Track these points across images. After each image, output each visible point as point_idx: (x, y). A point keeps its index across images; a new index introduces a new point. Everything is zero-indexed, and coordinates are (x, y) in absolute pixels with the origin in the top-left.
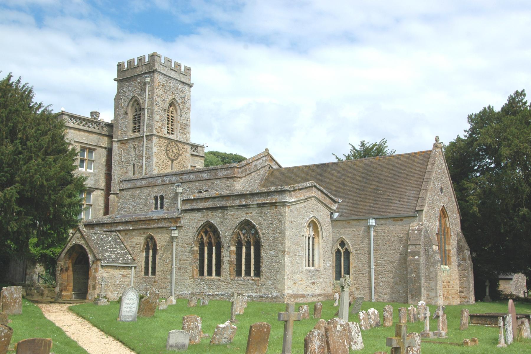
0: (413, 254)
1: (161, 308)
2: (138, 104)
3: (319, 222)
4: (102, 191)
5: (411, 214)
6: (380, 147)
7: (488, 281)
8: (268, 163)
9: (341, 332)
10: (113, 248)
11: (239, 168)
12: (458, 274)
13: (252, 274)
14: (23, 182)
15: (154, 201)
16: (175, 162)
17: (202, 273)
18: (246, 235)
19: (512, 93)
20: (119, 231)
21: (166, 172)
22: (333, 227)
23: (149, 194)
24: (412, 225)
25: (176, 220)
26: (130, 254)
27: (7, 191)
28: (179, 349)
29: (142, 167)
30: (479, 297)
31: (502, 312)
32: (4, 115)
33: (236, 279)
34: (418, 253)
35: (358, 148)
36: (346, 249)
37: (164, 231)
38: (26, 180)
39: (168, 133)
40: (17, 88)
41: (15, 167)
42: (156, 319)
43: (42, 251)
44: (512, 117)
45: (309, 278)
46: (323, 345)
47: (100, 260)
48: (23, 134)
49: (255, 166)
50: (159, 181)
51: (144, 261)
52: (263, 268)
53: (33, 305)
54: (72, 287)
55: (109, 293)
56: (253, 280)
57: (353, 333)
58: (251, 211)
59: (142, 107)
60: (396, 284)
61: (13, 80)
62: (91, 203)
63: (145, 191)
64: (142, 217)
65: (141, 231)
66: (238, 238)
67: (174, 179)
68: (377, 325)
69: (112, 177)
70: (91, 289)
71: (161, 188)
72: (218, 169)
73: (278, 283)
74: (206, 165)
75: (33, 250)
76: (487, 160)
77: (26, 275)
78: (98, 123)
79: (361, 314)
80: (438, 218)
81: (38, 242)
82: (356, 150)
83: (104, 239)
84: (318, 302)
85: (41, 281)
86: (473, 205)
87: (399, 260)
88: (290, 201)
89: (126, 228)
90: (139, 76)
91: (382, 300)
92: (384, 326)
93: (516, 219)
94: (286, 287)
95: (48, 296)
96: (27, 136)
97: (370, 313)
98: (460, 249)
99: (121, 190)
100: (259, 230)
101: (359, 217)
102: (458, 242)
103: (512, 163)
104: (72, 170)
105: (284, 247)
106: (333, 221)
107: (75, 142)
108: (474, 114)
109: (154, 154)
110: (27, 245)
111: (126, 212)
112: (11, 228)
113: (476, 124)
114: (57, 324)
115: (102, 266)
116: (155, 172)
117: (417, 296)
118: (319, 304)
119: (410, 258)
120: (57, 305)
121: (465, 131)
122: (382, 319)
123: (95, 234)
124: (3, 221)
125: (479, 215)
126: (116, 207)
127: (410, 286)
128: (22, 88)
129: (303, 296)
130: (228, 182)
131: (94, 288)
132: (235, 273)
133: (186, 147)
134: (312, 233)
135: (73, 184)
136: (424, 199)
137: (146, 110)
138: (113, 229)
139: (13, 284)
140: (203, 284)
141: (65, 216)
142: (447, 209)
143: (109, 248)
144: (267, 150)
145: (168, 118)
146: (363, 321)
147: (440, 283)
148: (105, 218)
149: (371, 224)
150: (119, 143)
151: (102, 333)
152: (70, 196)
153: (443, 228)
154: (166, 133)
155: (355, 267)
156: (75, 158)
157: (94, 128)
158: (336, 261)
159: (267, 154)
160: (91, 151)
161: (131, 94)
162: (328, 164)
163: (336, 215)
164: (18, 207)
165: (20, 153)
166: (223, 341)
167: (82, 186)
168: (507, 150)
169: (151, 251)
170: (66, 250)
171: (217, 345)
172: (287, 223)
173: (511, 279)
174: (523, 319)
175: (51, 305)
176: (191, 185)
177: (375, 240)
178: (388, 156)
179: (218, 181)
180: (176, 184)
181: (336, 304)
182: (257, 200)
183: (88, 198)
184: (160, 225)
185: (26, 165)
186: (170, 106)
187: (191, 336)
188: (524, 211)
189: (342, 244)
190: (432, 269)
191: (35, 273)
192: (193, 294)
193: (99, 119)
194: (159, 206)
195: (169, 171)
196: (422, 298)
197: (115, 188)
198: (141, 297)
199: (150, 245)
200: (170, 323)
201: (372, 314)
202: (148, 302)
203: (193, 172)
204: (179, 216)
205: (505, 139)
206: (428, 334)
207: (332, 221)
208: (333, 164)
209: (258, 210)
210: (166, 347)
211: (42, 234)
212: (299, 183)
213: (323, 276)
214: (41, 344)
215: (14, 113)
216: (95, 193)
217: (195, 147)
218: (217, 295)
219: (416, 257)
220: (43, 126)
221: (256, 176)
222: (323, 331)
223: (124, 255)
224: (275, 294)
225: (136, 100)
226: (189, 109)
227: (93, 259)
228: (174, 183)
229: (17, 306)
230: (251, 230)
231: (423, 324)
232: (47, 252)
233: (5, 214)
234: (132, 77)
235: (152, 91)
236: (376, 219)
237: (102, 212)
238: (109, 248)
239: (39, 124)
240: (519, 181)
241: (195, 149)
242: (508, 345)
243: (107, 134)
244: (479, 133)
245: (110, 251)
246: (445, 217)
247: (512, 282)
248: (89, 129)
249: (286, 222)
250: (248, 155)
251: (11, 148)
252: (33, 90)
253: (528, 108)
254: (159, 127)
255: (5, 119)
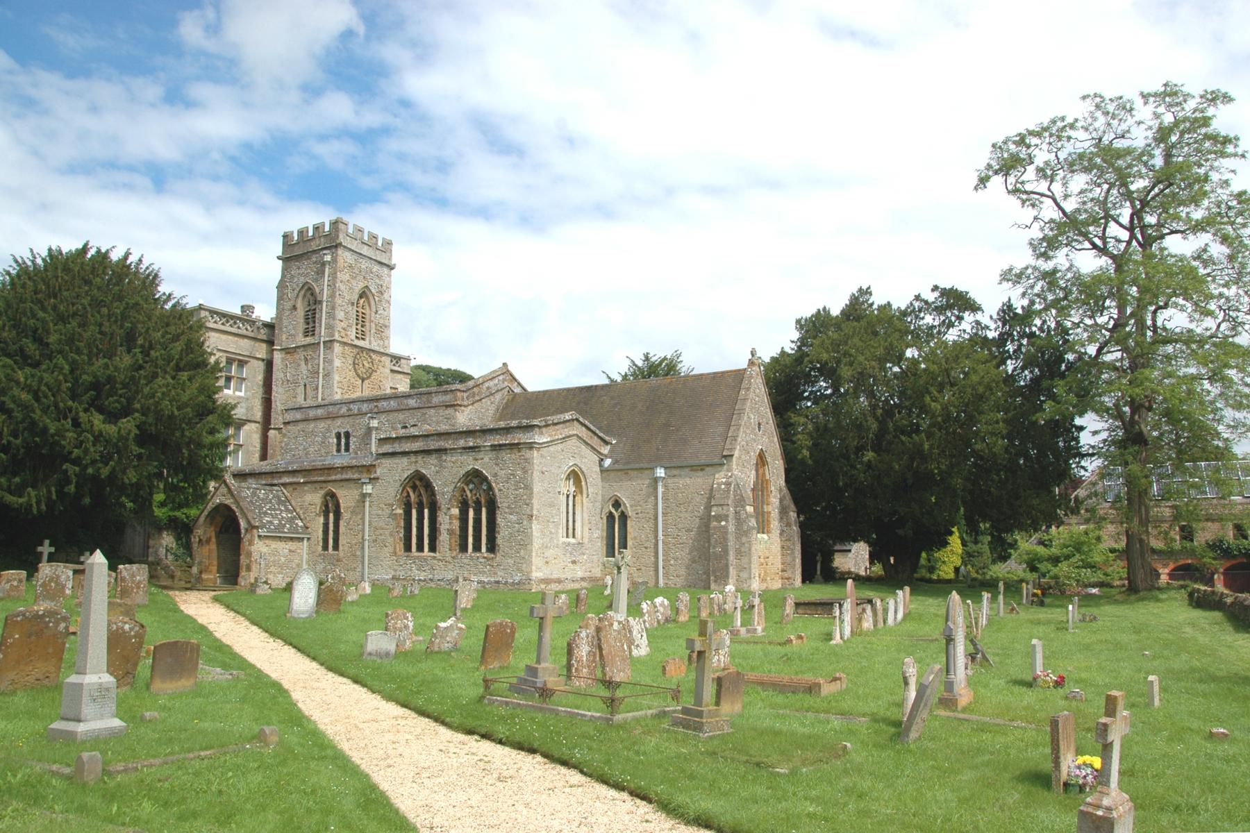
0: (719, 518)
1: (349, 599)
2: (312, 294)
3: (583, 472)
4: (257, 425)
5: (716, 460)
6: (671, 363)
7: (819, 554)
8: (506, 383)
9: (619, 632)
10: (275, 510)
11: (463, 391)
12: (780, 545)
13: (484, 549)
14: (145, 411)
15: (335, 440)
16: (366, 381)
17: (408, 548)
18: (474, 492)
19: (855, 291)
20: (284, 485)
21: (354, 396)
22: (603, 479)
23: (328, 430)
24: (717, 476)
25: (370, 468)
26: (301, 519)
27: (123, 423)
28: (381, 658)
29: (317, 389)
30: (808, 576)
31: (837, 597)
32: (119, 312)
33: (459, 556)
34: (726, 518)
35: (640, 363)
36: (623, 513)
37: (352, 485)
38: (148, 409)
39: (357, 337)
40: (137, 272)
41: (134, 388)
42: (342, 615)
43: (171, 514)
44: (855, 323)
45: (568, 555)
46: (594, 650)
47: (257, 527)
48: (145, 339)
49: (488, 388)
50: (344, 410)
51: (321, 529)
52: (499, 541)
53: (161, 592)
54: (216, 568)
55: (271, 576)
56: (484, 558)
57: (634, 633)
58: (481, 456)
59: (319, 299)
60: (694, 562)
61: (133, 259)
62: (241, 443)
63: (322, 425)
64: (319, 464)
65: (317, 486)
66: (462, 496)
67: (365, 407)
68: (667, 620)
69: (273, 404)
70: (244, 570)
71: (346, 420)
72: (431, 393)
73: (523, 562)
74: (412, 387)
75: (159, 512)
76: (822, 383)
77: (148, 547)
78: (253, 322)
79: (644, 606)
80: (754, 467)
81: (165, 500)
82: (636, 366)
83: (261, 496)
84: (582, 589)
85: (170, 557)
86: (803, 448)
87: (698, 528)
88: (541, 441)
89: (295, 480)
90: (314, 252)
91: (673, 586)
92: (677, 622)
93: (859, 466)
94: (534, 568)
95: (180, 580)
96: (150, 342)
97: (658, 605)
98: (783, 511)
99: (286, 423)
100: (494, 485)
101: (642, 465)
102: (781, 501)
103: (856, 389)
104: (215, 393)
105: (532, 510)
106: (603, 471)
107: (219, 350)
108: (804, 317)
109: (335, 368)
110: (151, 505)
111: (294, 455)
112: (128, 478)
113: (807, 331)
114: (200, 621)
115: (259, 536)
116: (338, 397)
117: (723, 578)
118: (583, 592)
119: (714, 524)
120: (195, 593)
121: (793, 342)
122: (674, 612)
123: (248, 488)
124: (117, 469)
125: (810, 462)
126: (278, 449)
127: (714, 564)
128: (145, 271)
129: (559, 581)
130: (447, 412)
131: (249, 569)
132: (458, 548)
133: (384, 358)
134: (573, 489)
135: (216, 415)
136: (735, 438)
137: (324, 304)
138: (276, 482)
139: (131, 562)
140: (411, 564)
141: (205, 461)
142: (766, 454)
143: (269, 509)
144: (505, 364)
145: (357, 316)
146: (647, 615)
147: (755, 558)
148: (262, 465)
149: (658, 475)
150: (284, 352)
151: (267, 635)
152: (212, 432)
153: (760, 481)
154: (354, 338)
155: (635, 538)
156: (220, 374)
157: (246, 329)
158: (607, 529)
159: (505, 371)
160: (242, 364)
161: (302, 280)
162: (596, 386)
163: (608, 462)
164: (137, 448)
165: (141, 367)
166: (446, 646)
167: (230, 417)
168: (848, 370)
169: (331, 515)
170: (206, 513)
171: (437, 653)
172: (536, 475)
173: (850, 551)
174: (864, 605)
175: (188, 592)
176: (392, 416)
177: (665, 499)
178: (684, 377)
179: (433, 411)
180: (369, 415)
181: (607, 592)
182: (490, 440)
183: (236, 435)
184: (344, 476)
185: (149, 385)
186: (361, 297)
187: (399, 640)
188: (869, 455)
189: (617, 504)
190: (744, 539)
191: (161, 545)
192: (394, 578)
193: (254, 316)
194: (343, 448)
195: (357, 394)
196: (730, 581)
197: (277, 420)
198: (321, 583)
199: (330, 505)
200: (364, 620)
201: (661, 605)
202: (331, 590)
203: (395, 397)
204: (374, 463)
205: (846, 354)
206: (738, 631)
207: (601, 471)
208: (603, 387)
209: (492, 455)
210: (362, 655)
211: (171, 489)
212: (552, 414)
213: (587, 552)
214: (187, 648)
215: (132, 308)
216: (246, 427)
217: (396, 359)
218: (431, 580)
219: (723, 523)
220: (173, 328)
221: (489, 403)
222: (592, 630)
223: (291, 520)
224: (517, 579)
225: (309, 289)
226: (389, 302)
227: (246, 526)
228: (366, 414)
229: (141, 593)
230: (482, 484)
231: (732, 617)
232: (178, 514)
233: (120, 458)
234: (305, 253)
235: (333, 276)
236: (666, 468)
237: (257, 455)
238: (269, 509)
239: (168, 325)
240: (864, 415)
241: (397, 362)
242: (844, 641)
243: (265, 339)
244: (811, 345)
245: (271, 514)
246: (764, 465)
247: (850, 555)
248: (240, 332)
249: (535, 472)
250: (476, 370)
251: (127, 360)
252: (161, 274)
253: (876, 312)
254: (344, 329)
255: (119, 318)
